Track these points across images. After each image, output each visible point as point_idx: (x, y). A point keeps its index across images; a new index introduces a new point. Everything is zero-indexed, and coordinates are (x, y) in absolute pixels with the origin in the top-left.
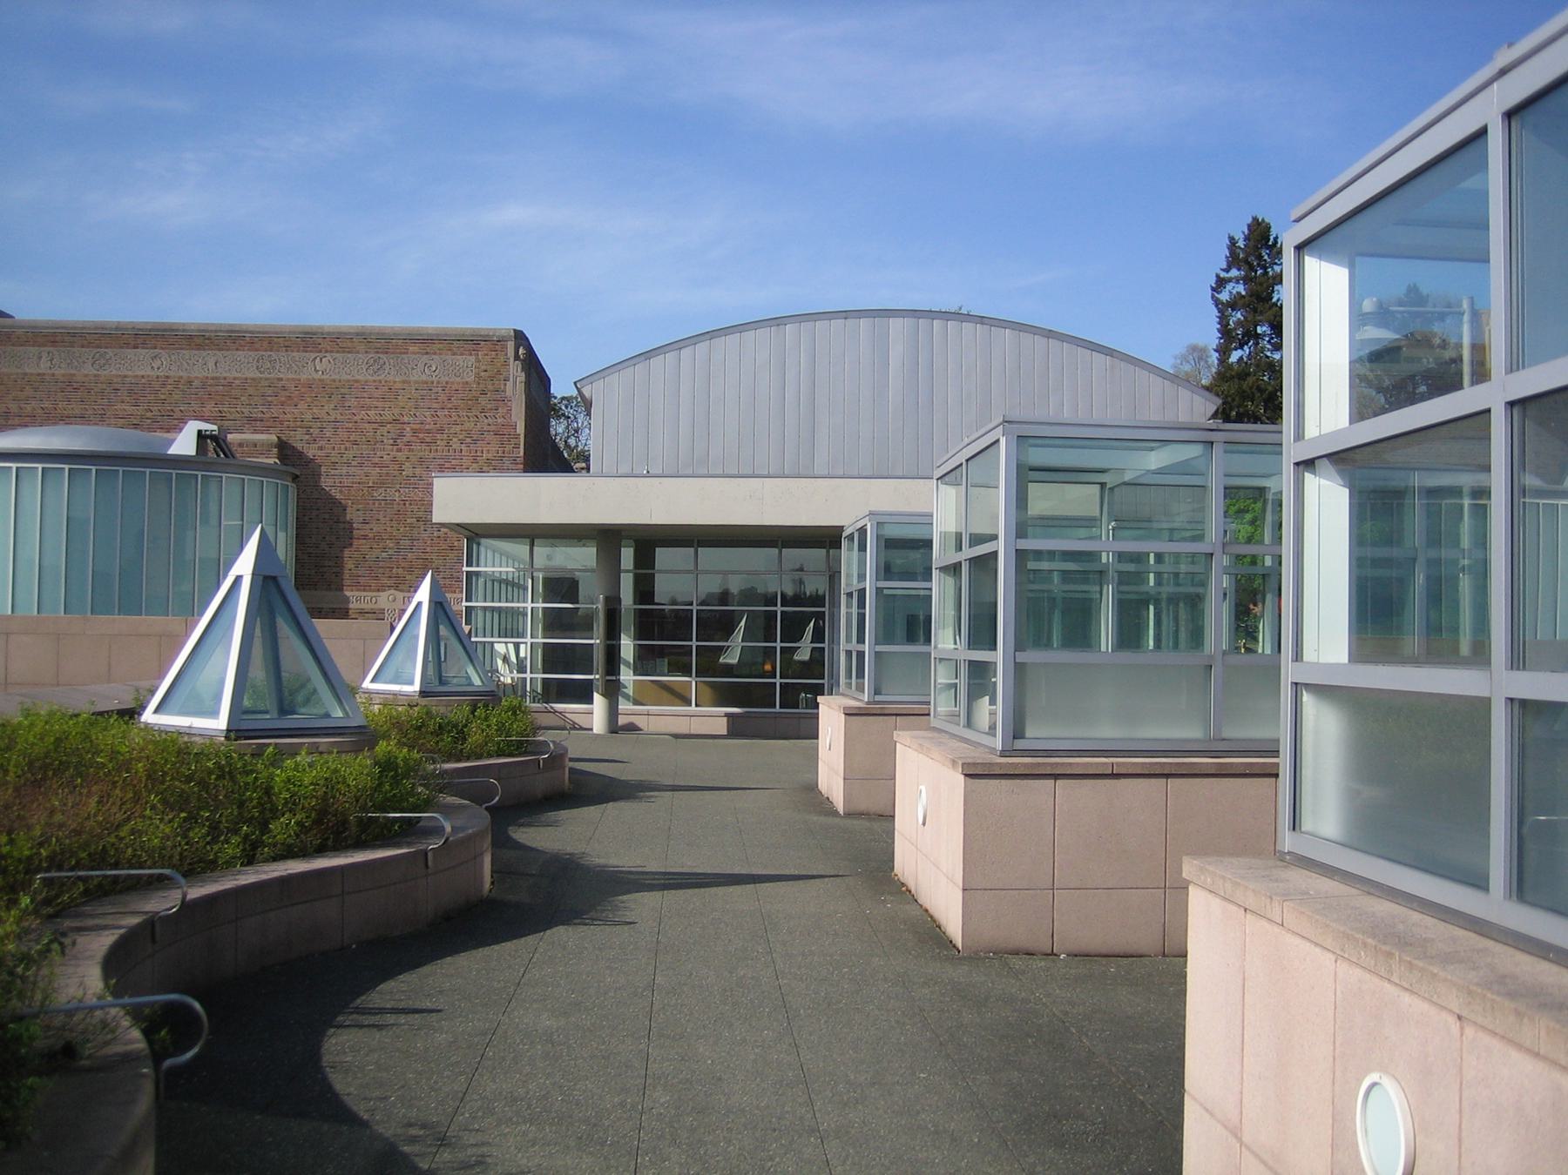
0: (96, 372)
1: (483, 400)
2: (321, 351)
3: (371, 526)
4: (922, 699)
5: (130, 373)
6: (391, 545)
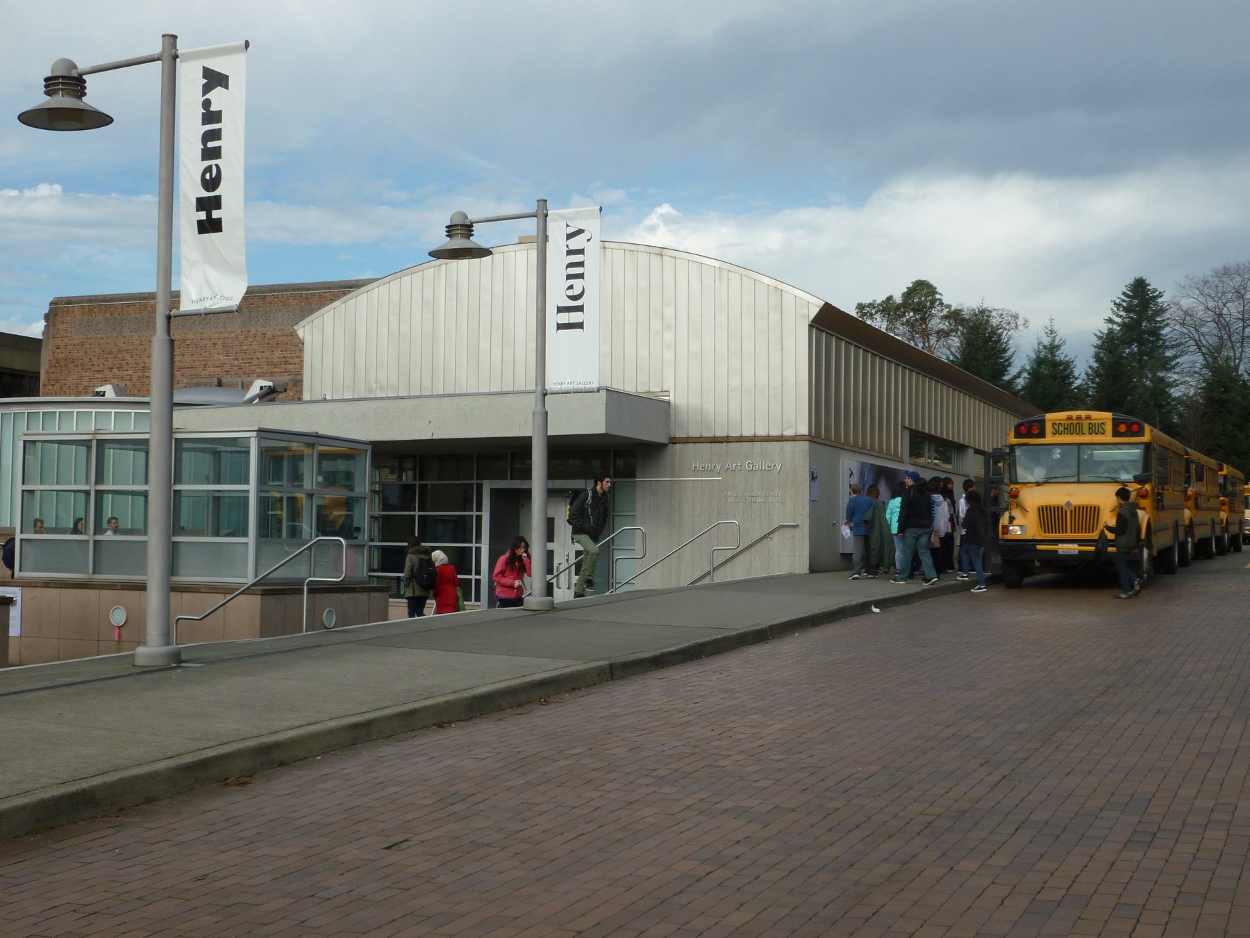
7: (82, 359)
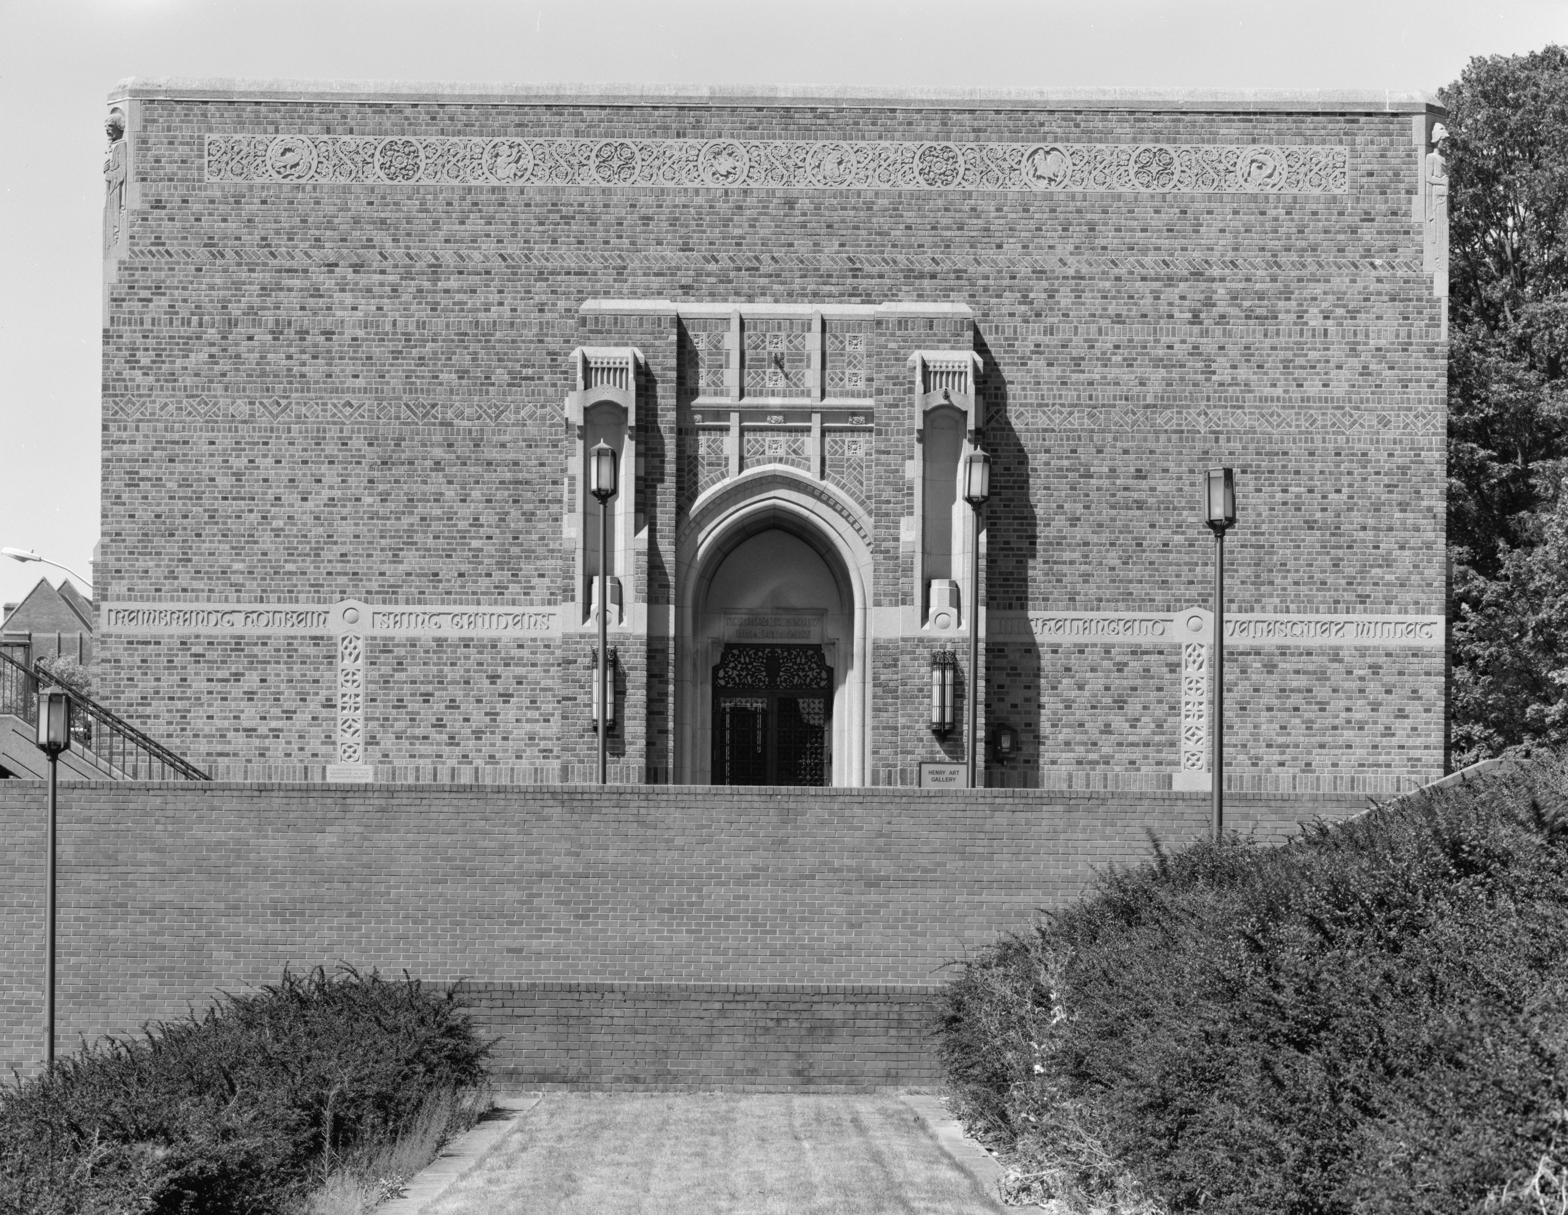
0: (604, 184)
1: (1367, 233)
2: (1045, 139)
3: (1152, 483)
4: (688, 771)
5: (671, 185)
6: (1191, 519)
7: (238, 239)
